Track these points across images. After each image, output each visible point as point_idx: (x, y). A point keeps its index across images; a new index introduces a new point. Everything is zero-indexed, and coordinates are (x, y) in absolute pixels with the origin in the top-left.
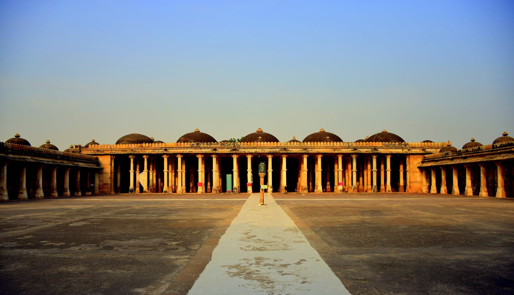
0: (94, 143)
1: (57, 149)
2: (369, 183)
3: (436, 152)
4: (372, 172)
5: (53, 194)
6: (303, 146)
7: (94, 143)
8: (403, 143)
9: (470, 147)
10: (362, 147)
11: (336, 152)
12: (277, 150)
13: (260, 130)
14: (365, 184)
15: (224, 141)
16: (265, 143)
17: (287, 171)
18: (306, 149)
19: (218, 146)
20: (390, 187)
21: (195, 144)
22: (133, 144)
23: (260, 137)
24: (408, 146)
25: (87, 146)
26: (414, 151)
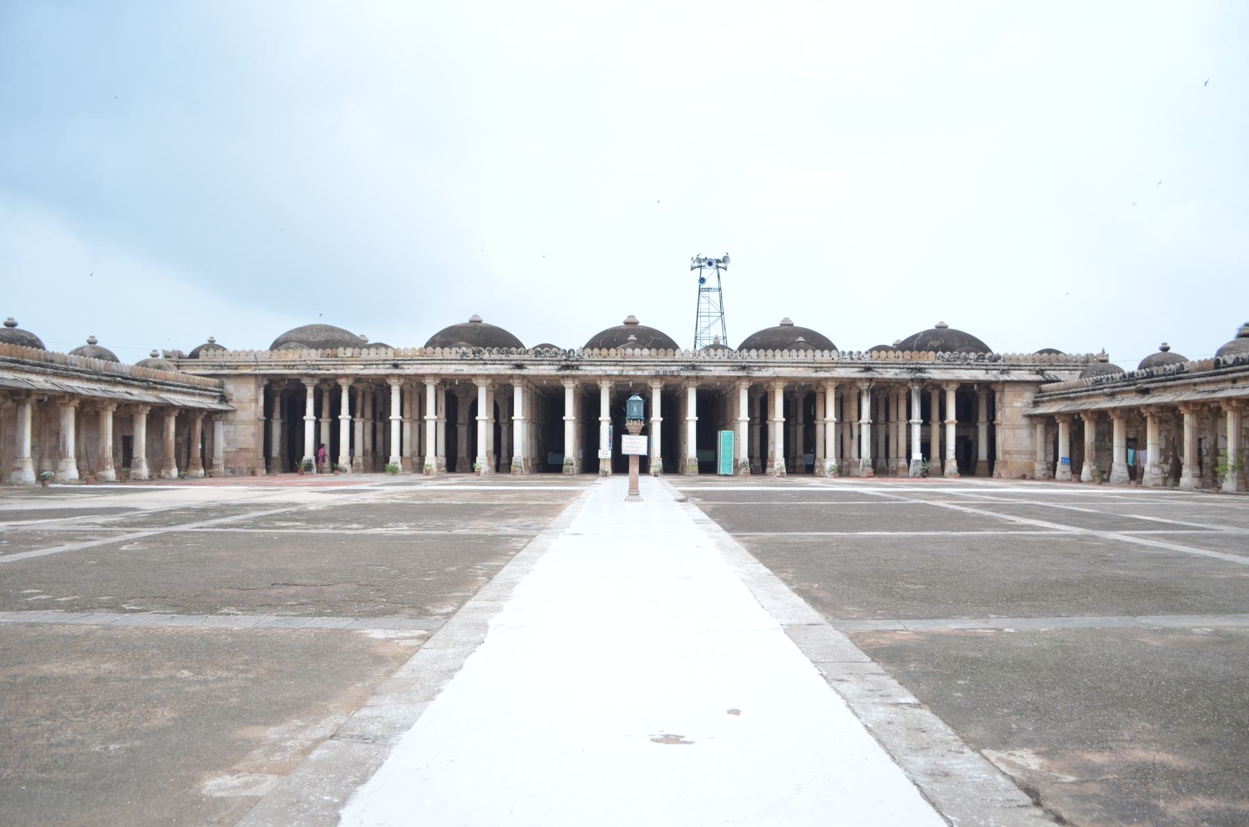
0: (211, 345)
1: (114, 359)
2: (903, 453)
3: (1069, 378)
4: (909, 426)
5: (101, 473)
6: (740, 359)
7: (211, 345)
8: (988, 355)
9: (1160, 364)
10: (887, 365)
11: (822, 374)
12: (673, 368)
13: (631, 320)
14: (892, 455)
15: (542, 346)
16: (646, 351)
17: (698, 422)
18: (744, 368)
19: (526, 357)
20: (954, 464)
21: (469, 351)
22: (313, 351)
23: (632, 337)
24: (1000, 362)
25: (194, 355)
26: (1015, 375)
